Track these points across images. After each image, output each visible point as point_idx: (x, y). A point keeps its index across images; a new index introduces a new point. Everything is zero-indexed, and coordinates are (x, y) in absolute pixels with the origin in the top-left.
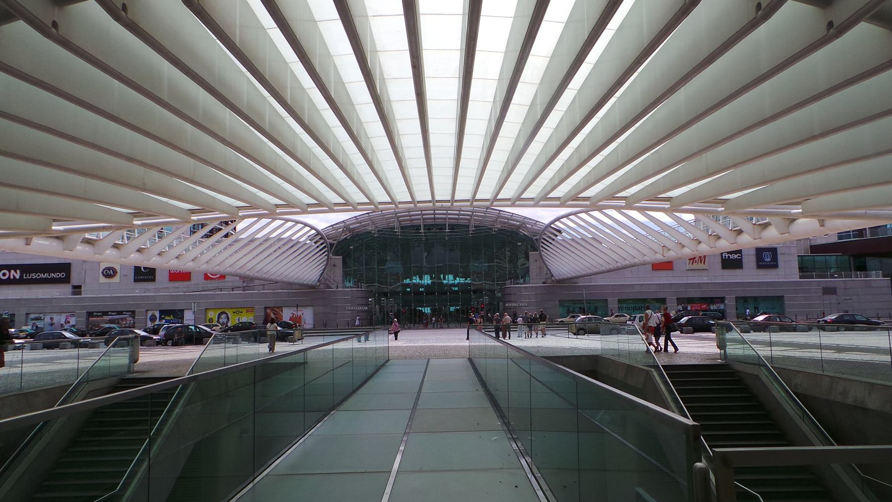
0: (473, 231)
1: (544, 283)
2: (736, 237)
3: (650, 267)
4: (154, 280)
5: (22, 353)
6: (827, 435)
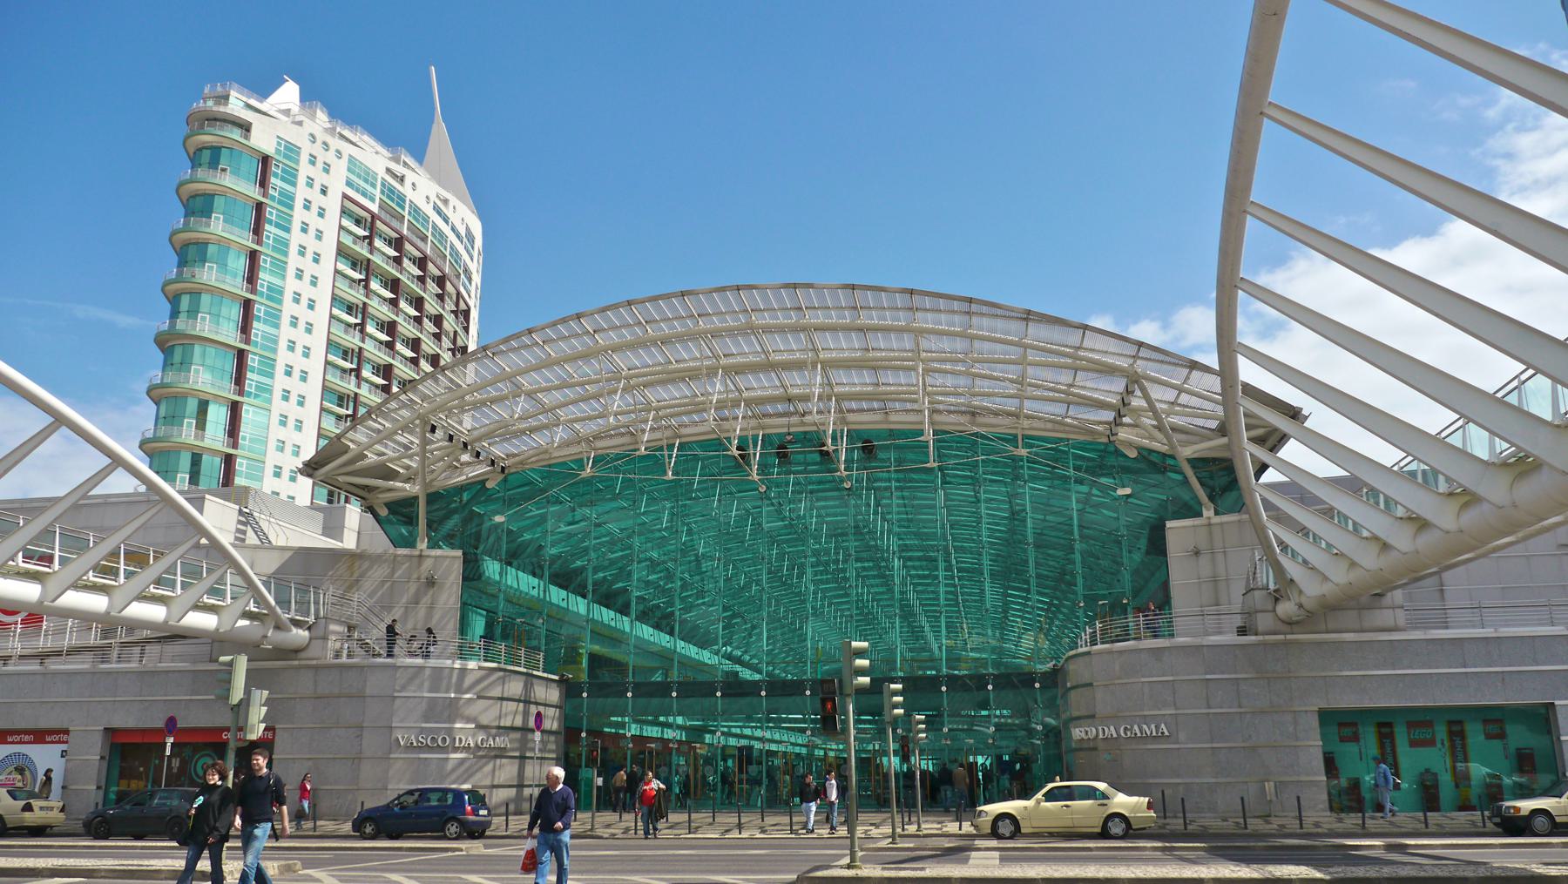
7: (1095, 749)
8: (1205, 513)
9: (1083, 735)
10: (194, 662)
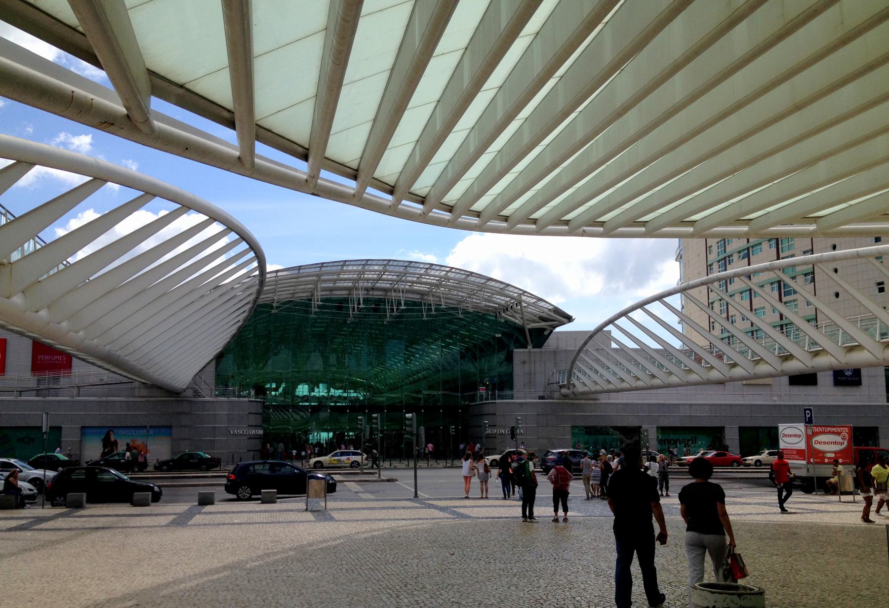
1: (541, 398)
2: (884, 349)
3: (785, 380)
7: (495, 437)
8: (529, 347)
9: (490, 432)
10: (128, 397)
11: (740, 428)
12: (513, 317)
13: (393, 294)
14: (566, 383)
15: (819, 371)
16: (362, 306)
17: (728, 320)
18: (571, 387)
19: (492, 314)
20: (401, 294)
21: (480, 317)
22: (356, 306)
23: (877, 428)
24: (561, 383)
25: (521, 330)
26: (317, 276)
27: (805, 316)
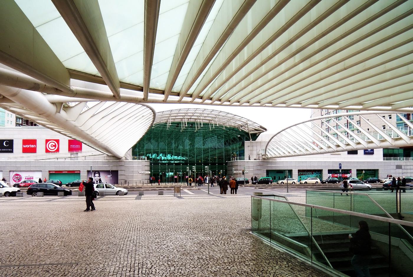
0: (170, 126)
3: (346, 152)
4: (12, 152)
5: (306, 194)
6: (405, 230)
11: (328, 170)
12: (244, 129)
13: (198, 120)
14: (264, 154)
15: (358, 150)
16: (186, 126)
17: (348, 128)
18: (266, 156)
19: (237, 128)
20: (201, 121)
21: (234, 130)
22: (184, 126)
23: (378, 170)
24: (262, 154)
25: (247, 134)
26: (169, 114)
27: (341, 131)
